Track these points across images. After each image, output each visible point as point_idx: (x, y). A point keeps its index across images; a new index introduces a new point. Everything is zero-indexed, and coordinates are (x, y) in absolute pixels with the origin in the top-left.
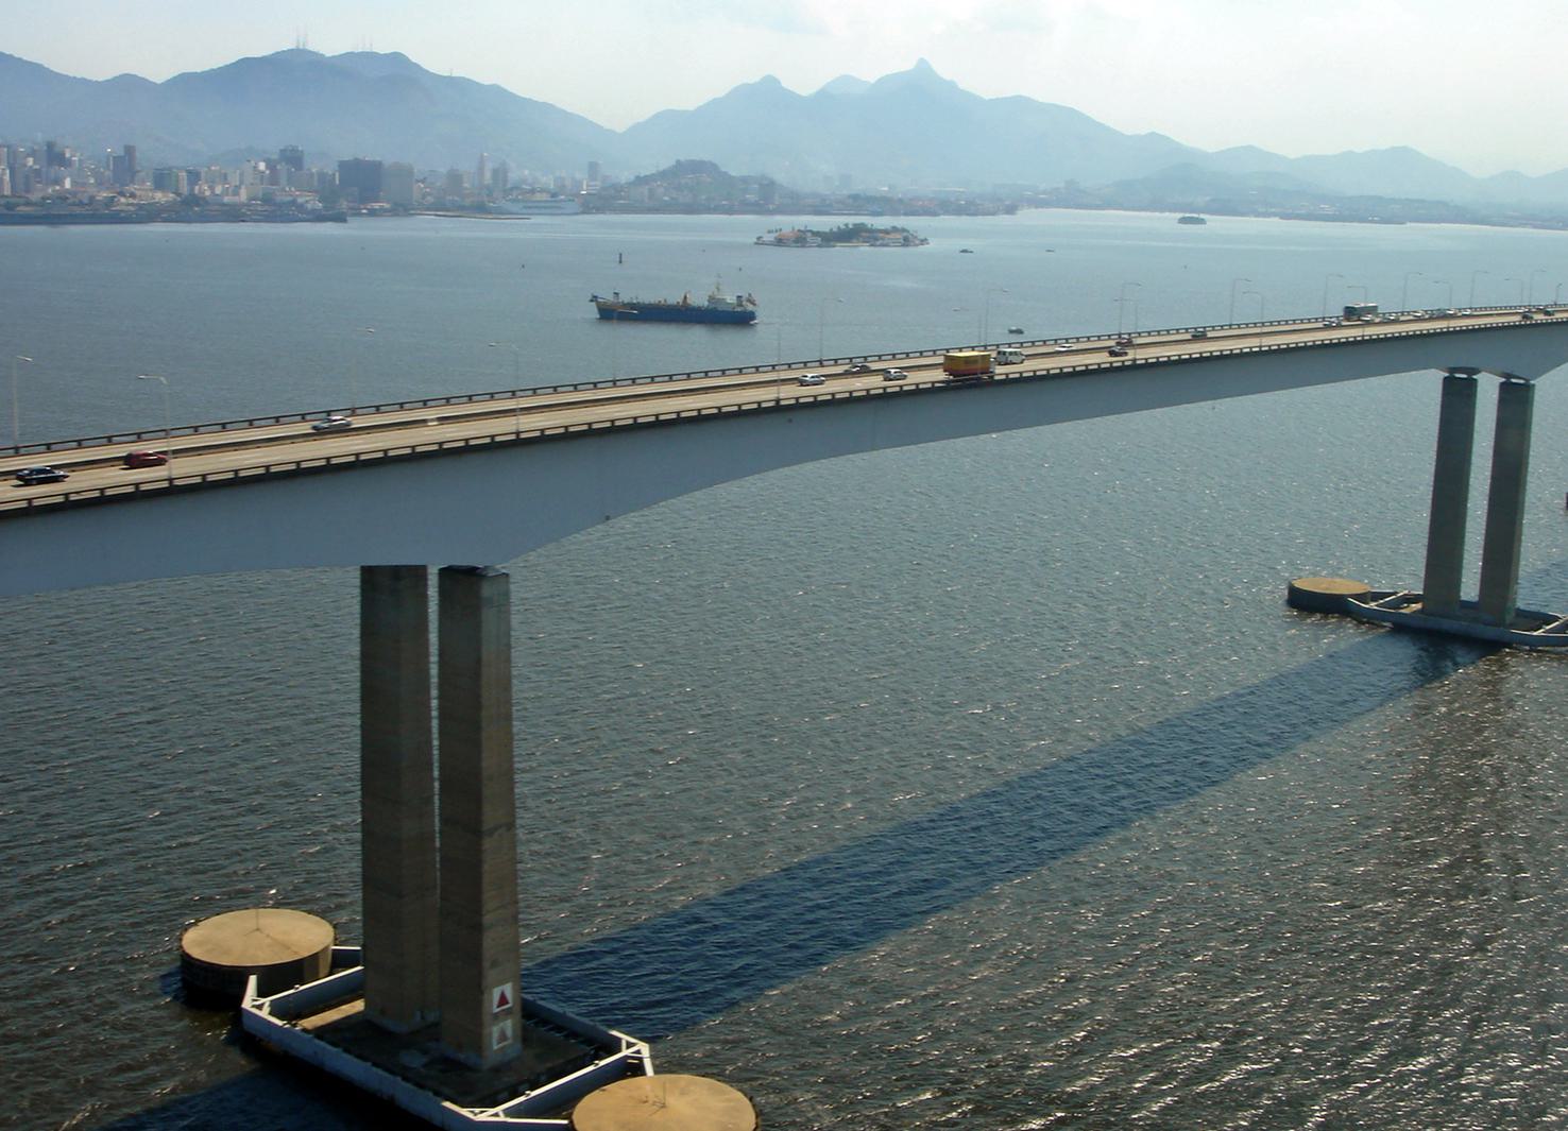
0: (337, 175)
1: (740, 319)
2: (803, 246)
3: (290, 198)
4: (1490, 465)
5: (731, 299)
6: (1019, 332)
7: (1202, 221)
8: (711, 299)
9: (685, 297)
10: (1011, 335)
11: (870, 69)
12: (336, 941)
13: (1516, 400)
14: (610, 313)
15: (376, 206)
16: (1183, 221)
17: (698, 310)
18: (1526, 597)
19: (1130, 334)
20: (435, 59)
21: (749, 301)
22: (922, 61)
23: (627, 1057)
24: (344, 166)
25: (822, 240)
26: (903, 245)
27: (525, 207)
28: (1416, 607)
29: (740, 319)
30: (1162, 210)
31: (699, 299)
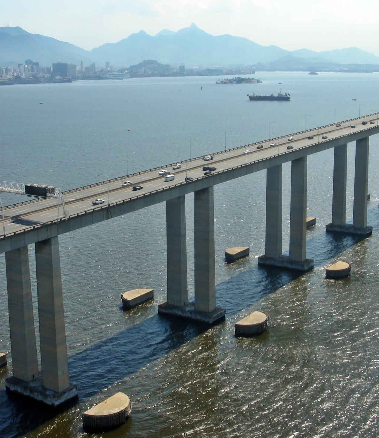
2: (232, 84)
4: (229, 181)
5: (284, 94)
7: (317, 74)
8: (279, 94)
9: (272, 94)
11: (175, 28)
16: (310, 74)
20: (30, 28)
21: (288, 95)
22: (193, 25)
25: (236, 82)
26: (258, 83)
31: (276, 95)
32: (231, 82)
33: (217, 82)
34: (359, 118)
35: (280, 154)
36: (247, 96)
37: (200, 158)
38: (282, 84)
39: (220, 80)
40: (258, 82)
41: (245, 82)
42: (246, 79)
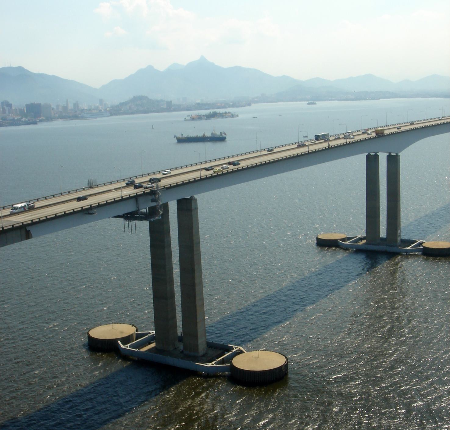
0: (25, 109)
1: (221, 139)
2: (201, 120)
3: (12, 118)
5: (218, 133)
6: (307, 137)
7: (315, 104)
8: (212, 134)
9: (204, 134)
10: (304, 138)
12: (137, 331)
13: (393, 161)
14: (181, 140)
15: (41, 118)
16: (309, 104)
17: (208, 138)
18: (404, 235)
19: (272, 148)
22: (203, 58)
23: (236, 351)
24: (28, 106)
26: (232, 117)
27: (91, 115)
28: (364, 241)
29: (221, 139)
30: (296, 101)
31: (208, 134)
32: (200, 118)
33: (185, 118)
34: (408, 122)
35: (264, 162)
36: (175, 137)
37: (296, 143)
38: (257, 118)
39: (190, 116)
40: (233, 116)
41: (219, 117)
42: (220, 113)
